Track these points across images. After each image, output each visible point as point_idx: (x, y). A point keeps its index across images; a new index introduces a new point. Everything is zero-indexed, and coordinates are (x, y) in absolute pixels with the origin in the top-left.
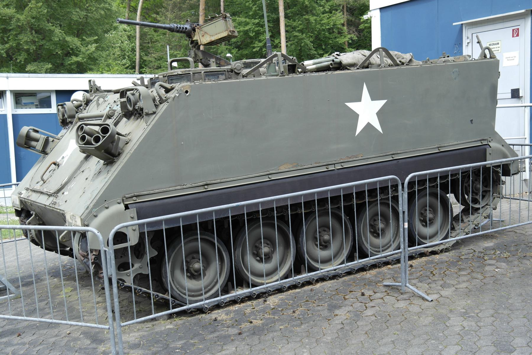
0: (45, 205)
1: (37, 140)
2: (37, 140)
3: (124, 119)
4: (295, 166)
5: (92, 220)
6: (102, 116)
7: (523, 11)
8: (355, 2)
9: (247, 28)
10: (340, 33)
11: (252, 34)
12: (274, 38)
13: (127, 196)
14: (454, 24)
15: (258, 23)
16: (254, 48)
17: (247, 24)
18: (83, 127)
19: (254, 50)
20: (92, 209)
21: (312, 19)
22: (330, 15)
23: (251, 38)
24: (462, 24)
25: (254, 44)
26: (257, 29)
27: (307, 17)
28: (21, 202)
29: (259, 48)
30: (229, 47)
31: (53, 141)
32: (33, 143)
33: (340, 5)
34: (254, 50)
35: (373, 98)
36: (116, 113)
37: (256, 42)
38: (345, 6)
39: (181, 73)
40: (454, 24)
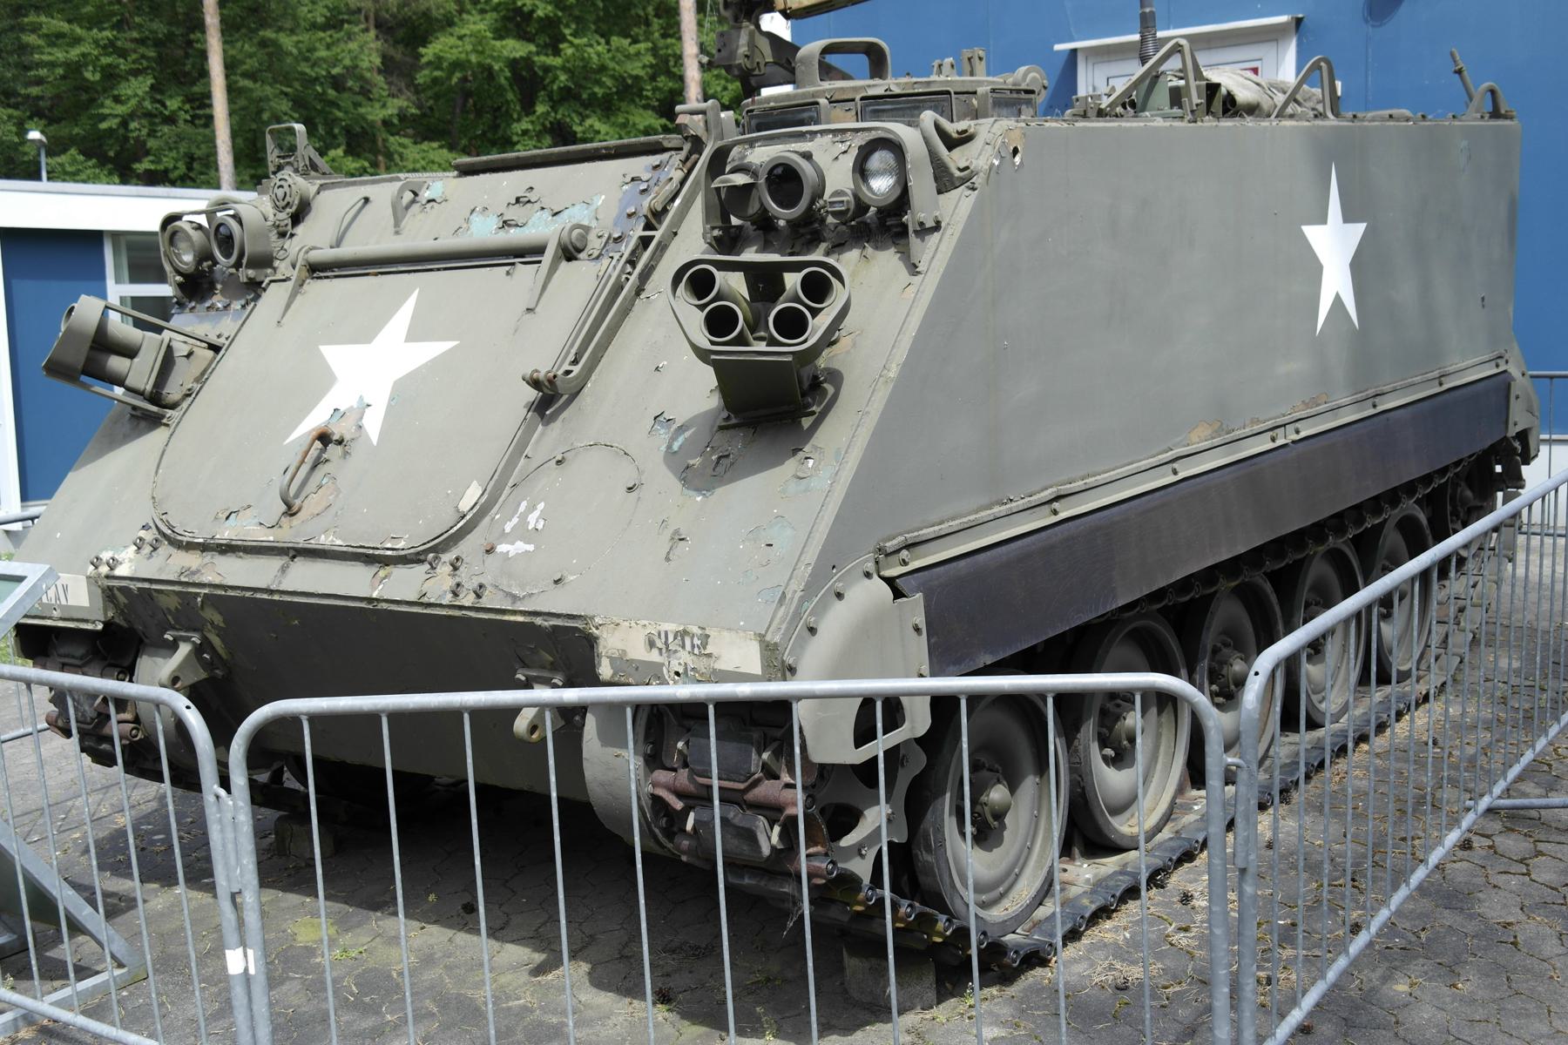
0: (370, 600)
1: (130, 352)
2: (130, 352)
3: (564, 264)
4: (1217, 433)
5: (801, 645)
6: (539, 250)
7: (1283, 19)
8: (405, 5)
9: (74, 53)
10: (365, 92)
11: (91, 75)
12: (162, 92)
13: (891, 545)
14: (1058, 47)
15: (112, 43)
16: (104, 118)
17: (77, 41)
18: (711, 279)
19: (104, 126)
20: (802, 600)
21: (287, 42)
22: (336, 36)
23: (86, 87)
24: (1074, 51)
25: (102, 106)
26: (105, 60)
27: (269, 34)
28: (109, 595)
29: (117, 121)
30: (16, 113)
31: (189, 356)
32: (116, 363)
33: (359, 10)
34: (104, 126)
35: (1348, 218)
36: (592, 237)
37: (108, 102)
38: (372, 16)
39: (897, 91)
40: (1058, 47)
